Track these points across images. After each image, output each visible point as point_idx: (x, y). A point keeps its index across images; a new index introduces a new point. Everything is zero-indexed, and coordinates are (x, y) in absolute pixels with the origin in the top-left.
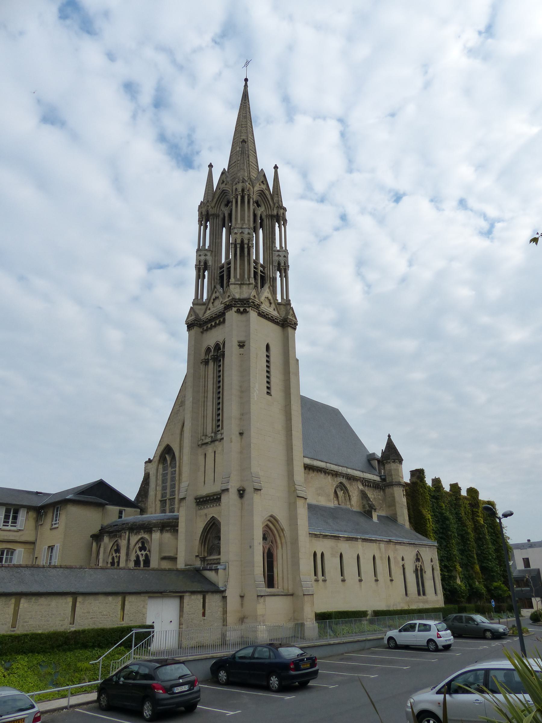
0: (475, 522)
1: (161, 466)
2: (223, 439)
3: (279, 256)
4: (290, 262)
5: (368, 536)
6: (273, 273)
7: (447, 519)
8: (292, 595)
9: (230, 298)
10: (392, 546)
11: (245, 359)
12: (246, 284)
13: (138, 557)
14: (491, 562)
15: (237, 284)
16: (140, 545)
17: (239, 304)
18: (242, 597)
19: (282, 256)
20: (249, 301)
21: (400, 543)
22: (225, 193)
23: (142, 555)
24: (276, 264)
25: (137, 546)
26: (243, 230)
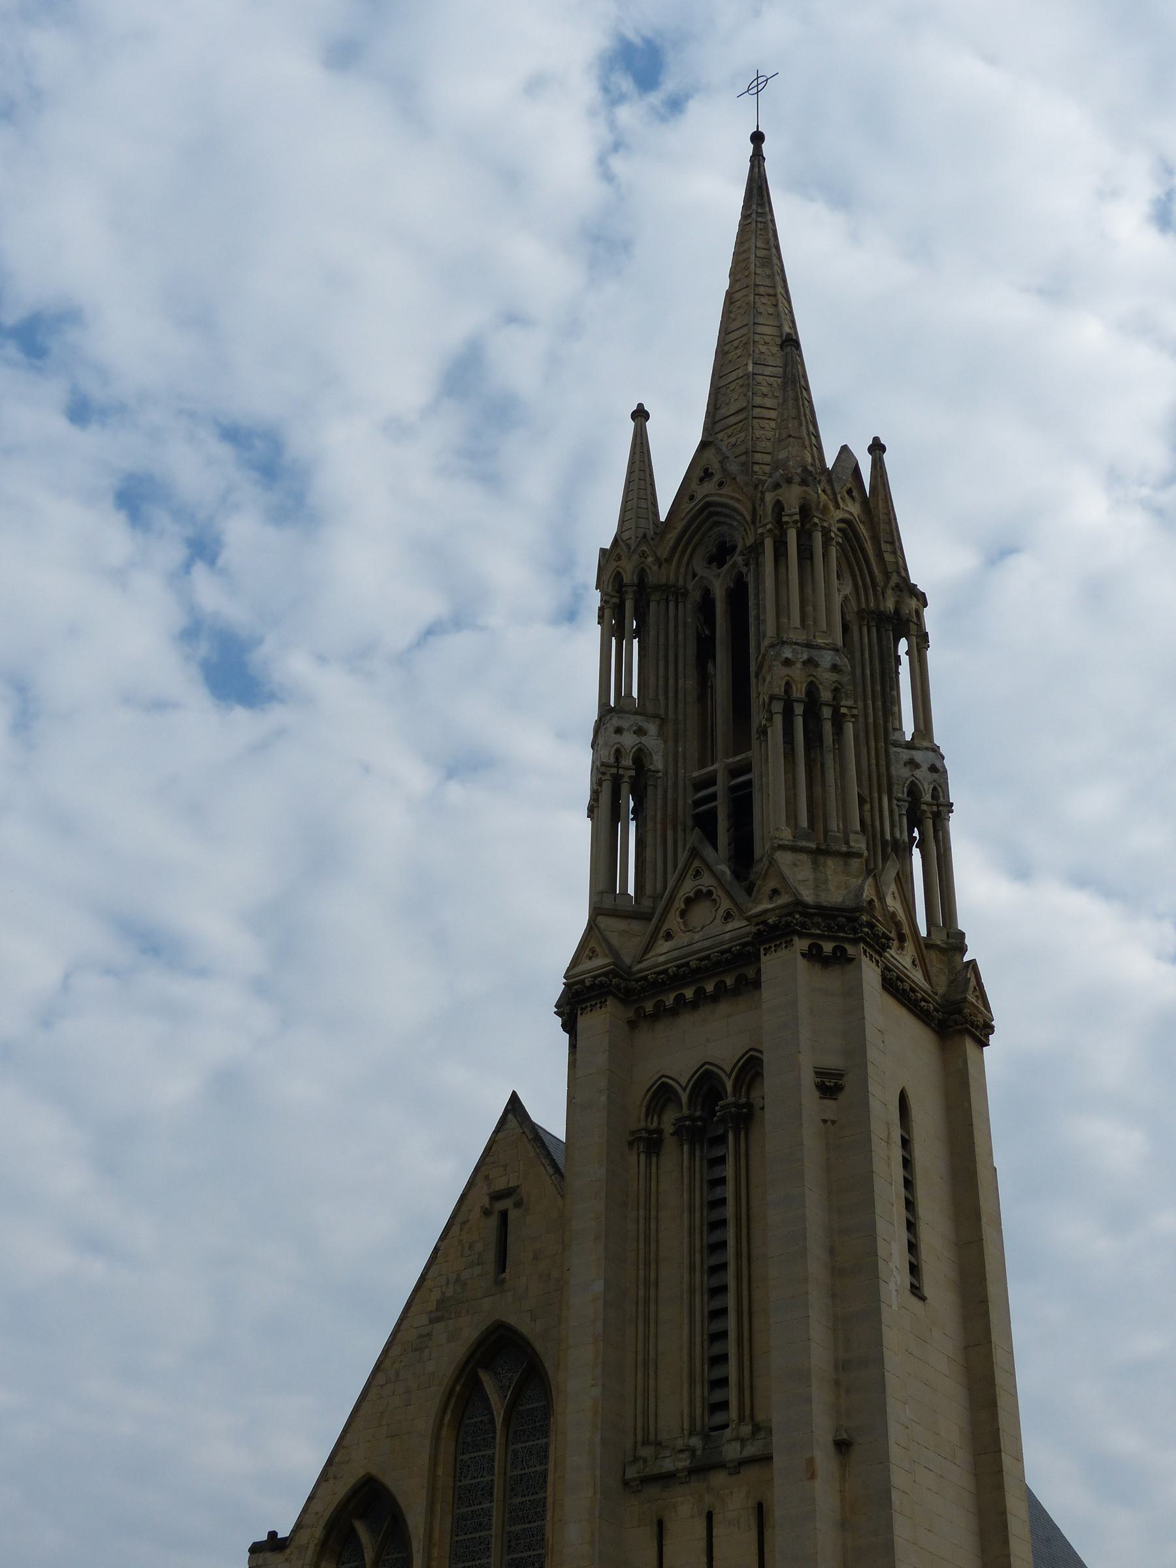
2: (765, 1459)
3: (912, 764)
9: (783, 900)
11: (847, 1141)
12: (838, 854)
17: (817, 926)
19: (925, 767)
20: (856, 919)
22: (712, 514)
24: (901, 792)
26: (814, 653)
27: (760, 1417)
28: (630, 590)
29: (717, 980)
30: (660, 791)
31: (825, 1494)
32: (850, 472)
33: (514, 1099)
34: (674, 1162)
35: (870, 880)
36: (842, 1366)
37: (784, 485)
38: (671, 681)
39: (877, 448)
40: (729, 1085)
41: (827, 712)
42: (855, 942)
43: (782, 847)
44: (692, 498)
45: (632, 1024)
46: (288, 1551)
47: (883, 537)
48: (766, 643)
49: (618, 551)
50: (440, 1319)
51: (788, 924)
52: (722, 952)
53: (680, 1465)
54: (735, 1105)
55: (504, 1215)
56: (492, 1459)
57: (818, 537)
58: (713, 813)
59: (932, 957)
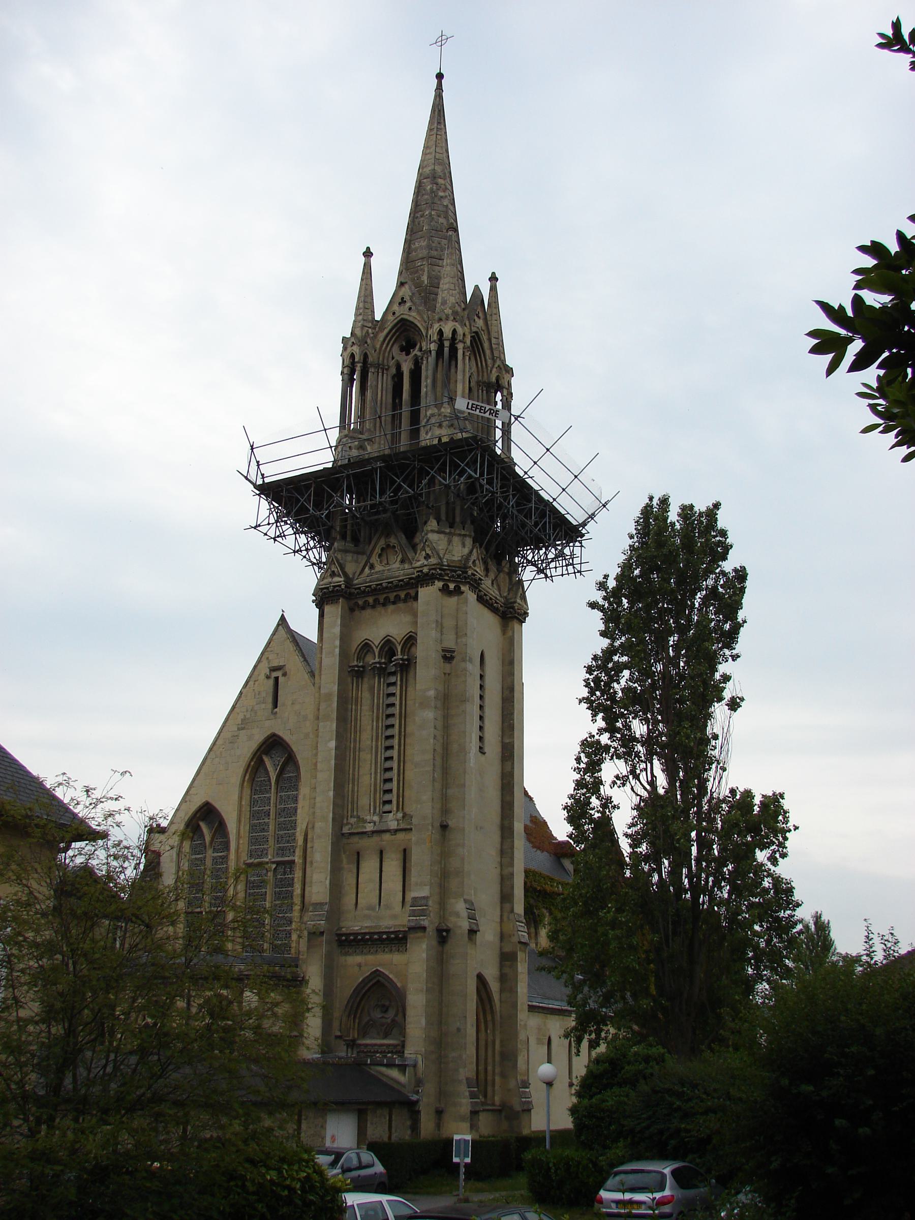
9: (433, 561)
27: (407, 810)
28: (359, 365)
29: (395, 594)
32: (479, 302)
33: (283, 618)
39: (493, 279)
44: (394, 313)
45: (352, 610)
50: (243, 729)
52: (400, 581)
54: (402, 659)
55: (277, 679)
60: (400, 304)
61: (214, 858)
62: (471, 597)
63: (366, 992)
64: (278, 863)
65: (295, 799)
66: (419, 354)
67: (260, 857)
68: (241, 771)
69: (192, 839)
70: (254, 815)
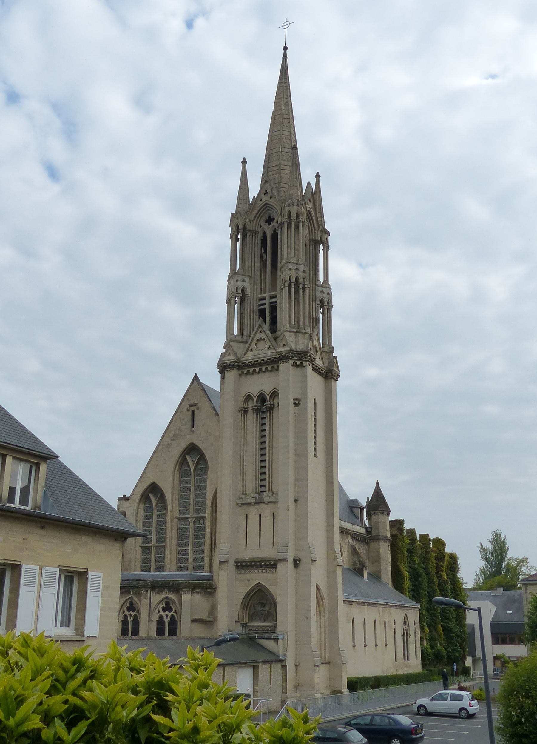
0: (440, 577)
1: (142, 506)
3: (322, 292)
4: (334, 302)
5: (371, 599)
6: (316, 313)
7: (420, 576)
8: (329, 663)
9: (286, 348)
10: (387, 609)
11: (300, 419)
13: (161, 617)
14: (451, 622)
15: (293, 332)
16: (164, 605)
17: (296, 356)
18: (296, 666)
19: (326, 293)
20: (306, 355)
21: (393, 606)
22: (267, 207)
23: (167, 616)
24: (318, 302)
25: (161, 606)
26: (298, 266)
27: (274, 490)
30: (249, 300)
31: (291, 514)
32: (310, 193)
33: (196, 376)
34: (251, 416)
35: (311, 342)
36: (297, 480)
37: (292, 206)
38: (253, 264)
39: (318, 176)
40: (268, 398)
41: (301, 286)
42: (306, 361)
43: (286, 331)
46: (129, 501)
47: (318, 210)
48: (284, 261)
49: (237, 216)
50: (174, 440)
51: (288, 356)
52: (268, 359)
53: (253, 501)
55: (193, 411)
56: (190, 480)
57: (301, 224)
58: (264, 310)
59: (324, 354)
60: (265, 194)
61: (158, 515)
62: (309, 369)
63: (252, 596)
64: (196, 518)
65: (205, 481)
66: (276, 224)
67: (186, 514)
68: (173, 465)
69: (145, 504)
70: (181, 490)
